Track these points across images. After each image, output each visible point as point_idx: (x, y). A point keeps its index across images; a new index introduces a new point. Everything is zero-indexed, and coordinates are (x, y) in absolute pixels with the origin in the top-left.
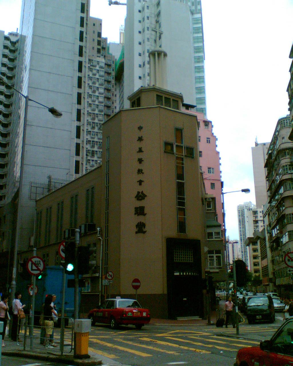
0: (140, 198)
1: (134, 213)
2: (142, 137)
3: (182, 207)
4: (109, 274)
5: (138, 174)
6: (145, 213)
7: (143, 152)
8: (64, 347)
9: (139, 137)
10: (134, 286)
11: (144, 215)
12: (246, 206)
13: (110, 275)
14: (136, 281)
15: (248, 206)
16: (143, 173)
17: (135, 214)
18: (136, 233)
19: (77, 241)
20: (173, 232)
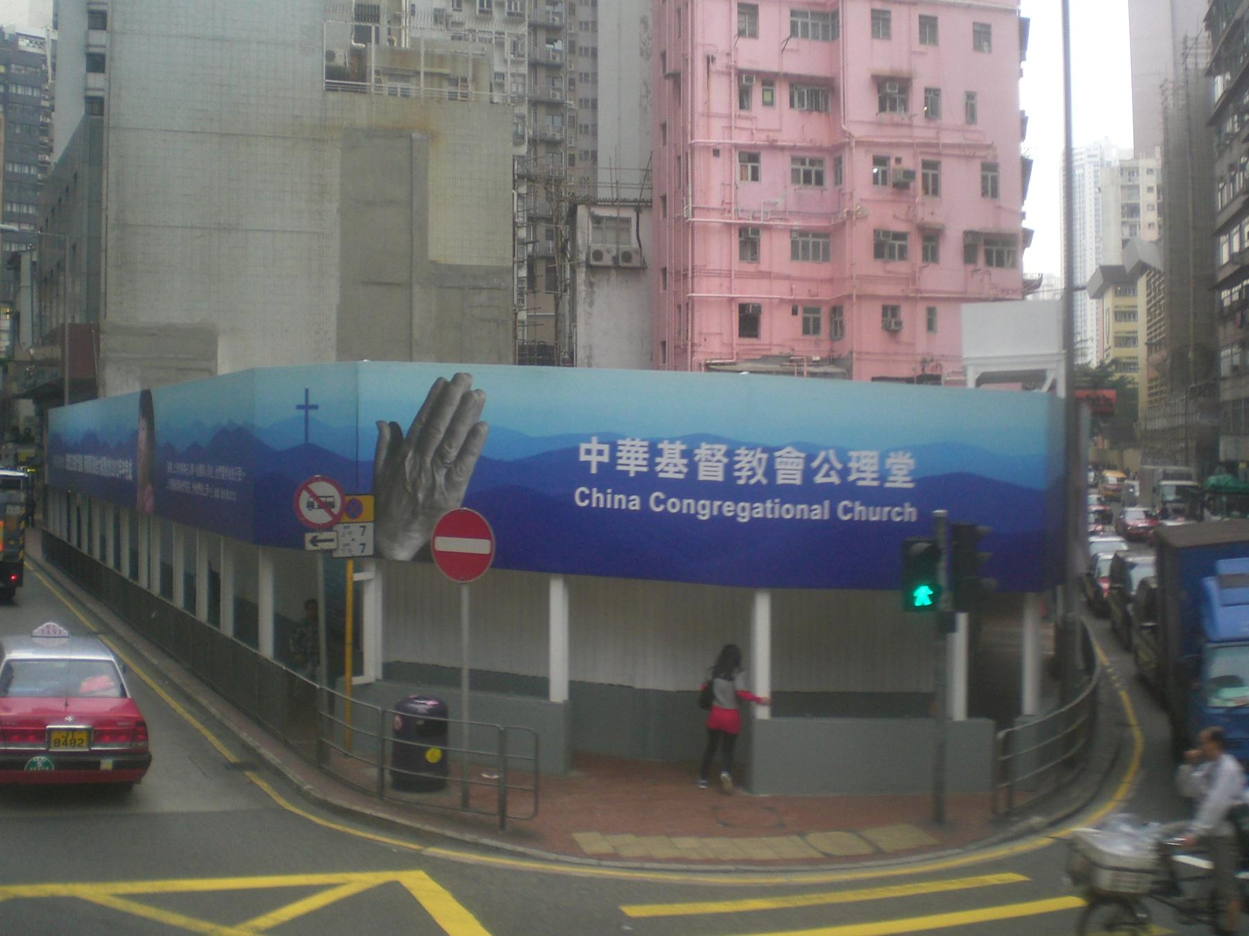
4: (310, 492)
8: (702, 476)
12: (1093, 152)
13: (317, 498)
15: (1098, 152)
19: (710, 274)
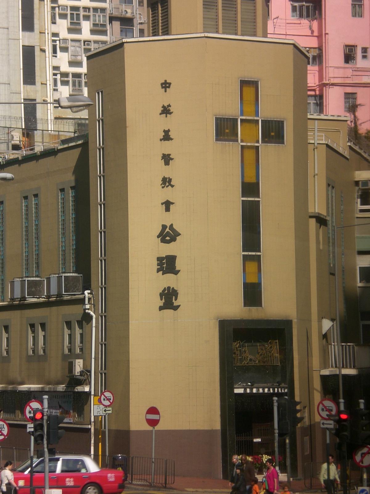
0: (168, 238)
1: (156, 267)
2: (169, 106)
3: (254, 253)
4: (104, 395)
5: (163, 187)
6: (177, 269)
7: (172, 139)
9: (163, 107)
10: (158, 414)
11: (176, 273)
14: (153, 410)
16: (172, 186)
17: (158, 271)
18: (161, 308)
20: (235, 308)
